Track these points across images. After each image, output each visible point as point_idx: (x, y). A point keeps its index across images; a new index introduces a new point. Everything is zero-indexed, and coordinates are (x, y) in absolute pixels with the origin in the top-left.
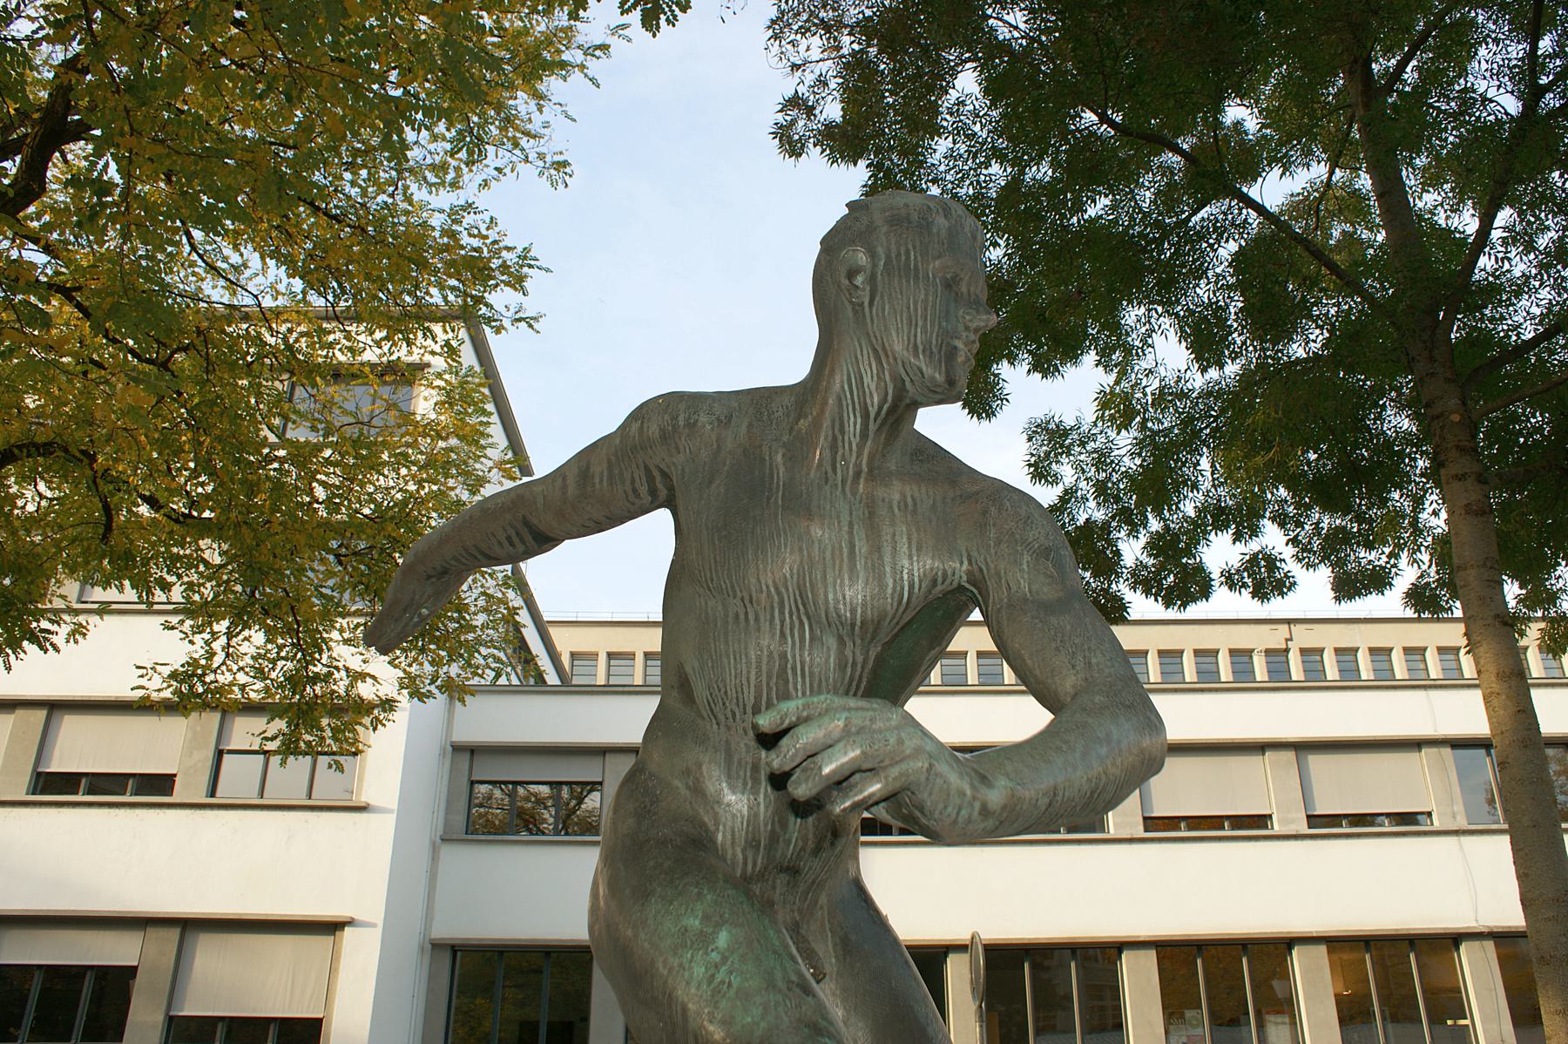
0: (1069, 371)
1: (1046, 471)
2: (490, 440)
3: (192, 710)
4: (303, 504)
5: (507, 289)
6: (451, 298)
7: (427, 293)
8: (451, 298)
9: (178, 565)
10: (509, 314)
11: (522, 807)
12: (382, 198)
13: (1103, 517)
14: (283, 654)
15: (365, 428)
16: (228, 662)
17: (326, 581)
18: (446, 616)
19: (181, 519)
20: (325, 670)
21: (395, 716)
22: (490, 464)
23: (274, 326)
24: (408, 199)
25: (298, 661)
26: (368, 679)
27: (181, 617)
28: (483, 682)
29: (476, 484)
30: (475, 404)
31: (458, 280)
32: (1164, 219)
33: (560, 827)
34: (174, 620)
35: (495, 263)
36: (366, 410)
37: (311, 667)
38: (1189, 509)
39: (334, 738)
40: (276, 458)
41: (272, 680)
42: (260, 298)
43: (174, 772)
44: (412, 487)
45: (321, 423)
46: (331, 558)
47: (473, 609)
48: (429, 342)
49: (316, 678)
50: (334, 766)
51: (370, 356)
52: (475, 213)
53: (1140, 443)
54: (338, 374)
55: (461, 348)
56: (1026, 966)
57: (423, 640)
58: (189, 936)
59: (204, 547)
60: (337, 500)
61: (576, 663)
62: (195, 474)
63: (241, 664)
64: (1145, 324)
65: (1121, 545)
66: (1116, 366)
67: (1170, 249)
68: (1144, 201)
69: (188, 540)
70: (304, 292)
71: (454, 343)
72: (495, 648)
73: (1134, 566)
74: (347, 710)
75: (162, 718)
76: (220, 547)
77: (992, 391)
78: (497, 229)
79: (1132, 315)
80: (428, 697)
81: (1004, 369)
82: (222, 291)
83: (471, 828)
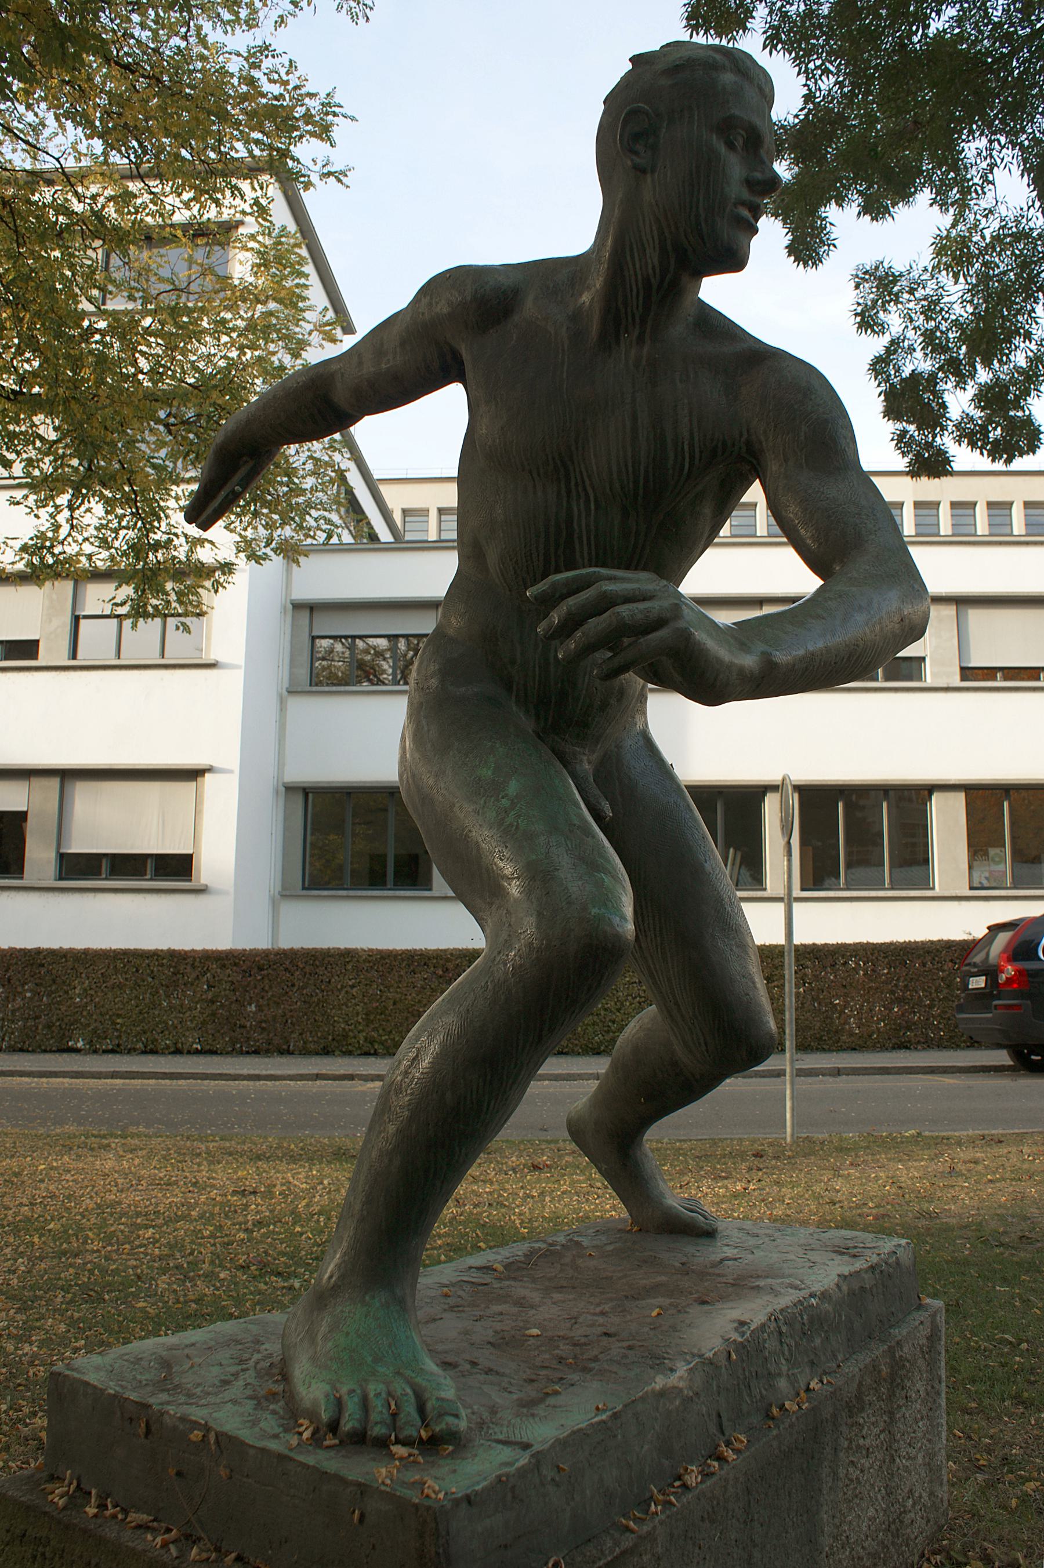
0: (901, 211)
1: (873, 320)
2: (308, 303)
3: (45, 580)
4: (128, 376)
5: (313, 140)
6: (257, 152)
7: (232, 148)
8: (257, 152)
9: (16, 442)
10: (317, 168)
11: (362, 659)
12: (176, 41)
13: (930, 368)
14: (124, 523)
15: (184, 296)
16: (73, 534)
17: (158, 451)
18: (275, 481)
19: (12, 397)
20: (165, 537)
21: (235, 578)
22: (310, 327)
23: (80, 189)
24: (203, 41)
25: (140, 530)
26: (206, 544)
27: (25, 492)
28: (315, 542)
29: (297, 348)
30: (292, 266)
31: (262, 132)
32: (1016, 30)
33: (399, 677)
34: (18, 494)
35: (299, 111)
36: (183, 274)
37: (151, 535)
38: (1020, 359)
39: (180, 602)
40: (98, 331)
41: (116, 549)
42: (62, 161)
43: (37, 638)
44: (234, 354)
45: (138, 291)
46: (161, 428)
47: (301, 472)
48: (238, 201)
49: (157, 546)
50: (181, 628)
51: (181, 217)
52: (273, 56)
53: (972, 290)
54: (149, 238)
55: (271, 206)
56: (840, 805)
57: (255, 505)
58: (68, 785)
59: (38, 423)
60: (161, 370)
61: (407, 519)
62: (20, 352)
63: (86, 535)
64: (985, 159)
65: (947, 397)
66: (952, 205)
67: (1019, 68)
68: (995, 9)
69: (22, 416)
70: (105, 154)
71: (264, 202)
72: (325, 510)
73: (959, 419)
74: (189, 575)
75: (18, 588)
76: (53, 423)
77: (818, 236)
78: (297, 74)
79: (972, 147)
80: (264, 559)
81: (831, 212)
82: (24, 155)
83: (314, 679)
